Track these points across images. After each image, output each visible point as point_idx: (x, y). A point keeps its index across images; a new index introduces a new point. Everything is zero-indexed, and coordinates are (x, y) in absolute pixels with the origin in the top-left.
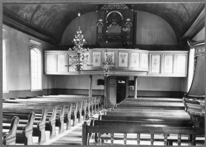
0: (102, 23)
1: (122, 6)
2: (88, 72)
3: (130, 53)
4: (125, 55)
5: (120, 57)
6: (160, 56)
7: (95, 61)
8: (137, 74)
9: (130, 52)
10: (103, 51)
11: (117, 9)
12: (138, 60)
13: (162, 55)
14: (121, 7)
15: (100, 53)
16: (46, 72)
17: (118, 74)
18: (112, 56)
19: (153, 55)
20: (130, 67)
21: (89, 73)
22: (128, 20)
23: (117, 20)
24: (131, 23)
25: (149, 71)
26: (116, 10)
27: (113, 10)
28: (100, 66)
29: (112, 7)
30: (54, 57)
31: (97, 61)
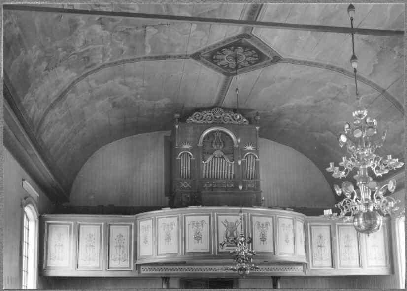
0: (190, 153)
1: (235, 118)
2: (159, 267)
3: (276, 219)
4: (267, 224)
5: (255, 227)
6: (328, 228)
7: (193, 239)
8: (280, 271)
9: (276, 216)
10: (214, 212)
11: (223, 123)
12: (291, 237)
13: (335, 225)
14: (232, 120)
15: (206, 218)
16: (47, 270)
17: (220, 271)
18: (237, 224)
19: (314, 226)
20: (278, 254)
21: (164, 272)
22: (186, 146)
23: (223, 147)
24: (191, 154)
25: (308, 263)
26: (222, 125)
27: (214, 125)
28: (209, 250)
29: (212, 118)
30: (70, 233)
31: (198, 238)
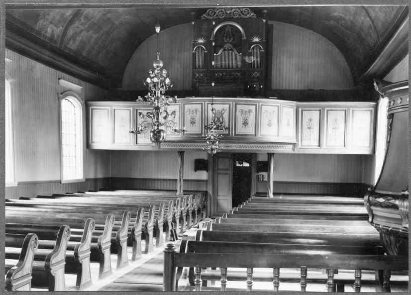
0: (203, 46)
1: (244, 13)
2: (175, 144)
3: (259, 106)
4: (250, 111)
5: (239, 114)
6: (318, 112)
7: (189, 123)
8: (273, 149)
9: (259, 104)
10: (205, 102)
11: (232, 18)
12: (274, 121)
13: (324, 110)
14: (241, 15)
15: (199, 106)
16: (92, 144)
17: (235, 148)
18: (223, 112)
19: (305, 110)
20: (259, 135)
21: (178, 147)
23: (233, 41)
25: (297, 143)
26: (232, 19)
27: (225, 20)
28: (200, 133)
29: (223, 13)
30: (108, 115)
31: (193, 122)
